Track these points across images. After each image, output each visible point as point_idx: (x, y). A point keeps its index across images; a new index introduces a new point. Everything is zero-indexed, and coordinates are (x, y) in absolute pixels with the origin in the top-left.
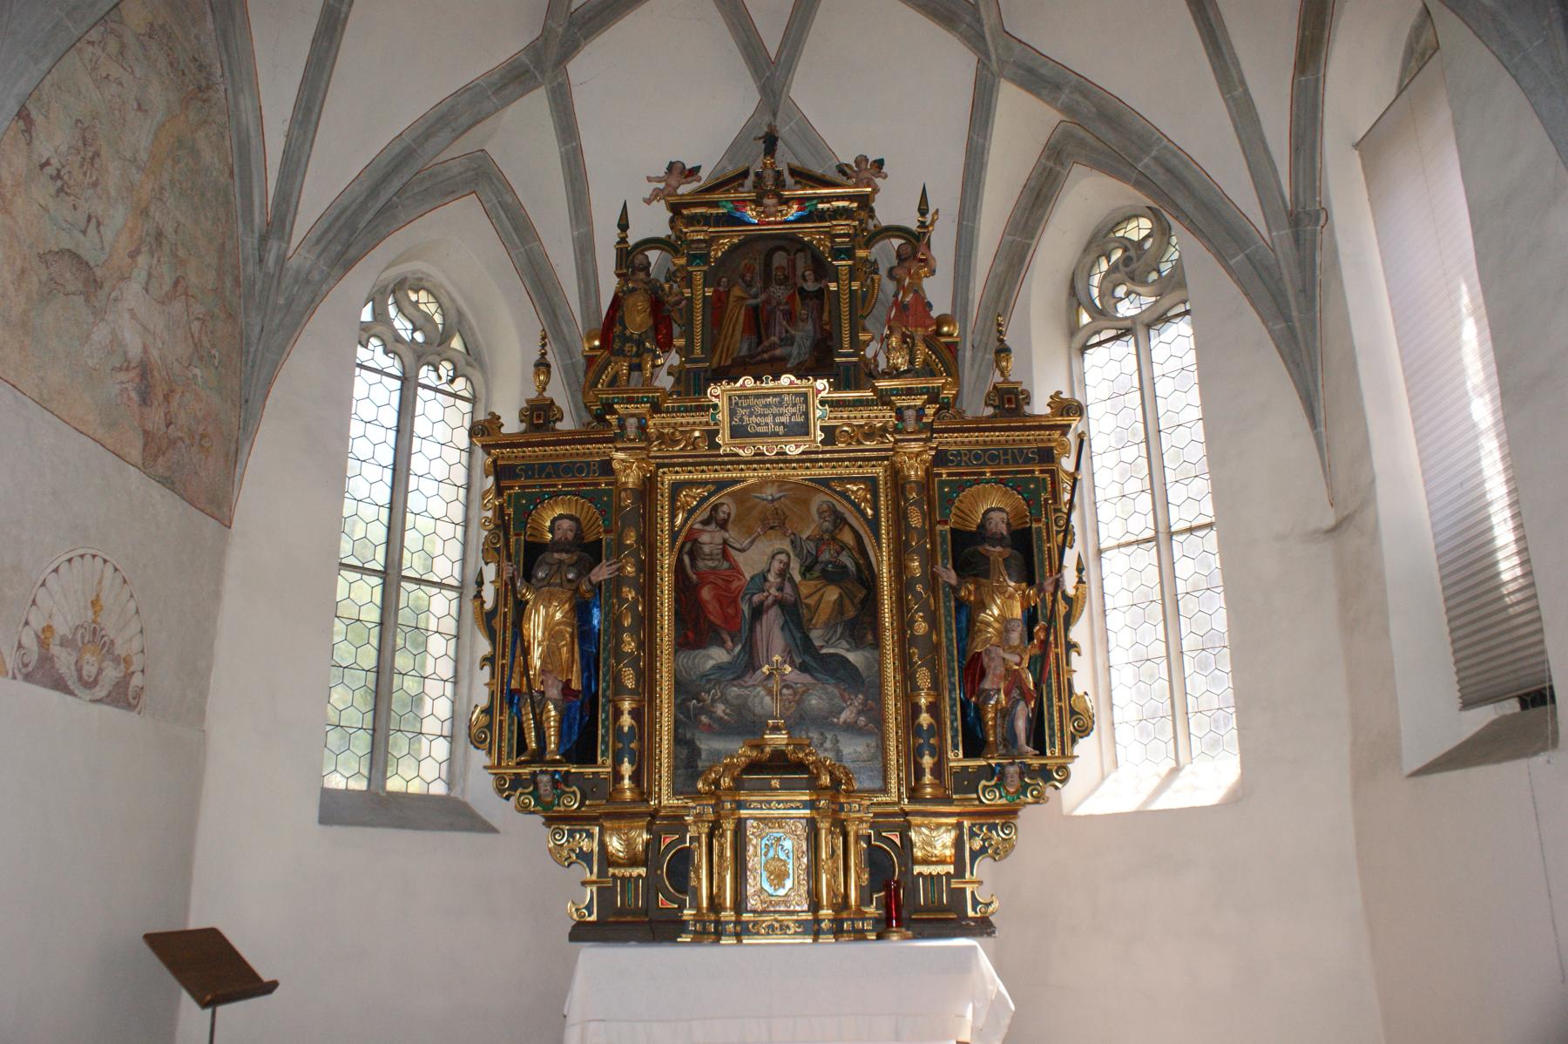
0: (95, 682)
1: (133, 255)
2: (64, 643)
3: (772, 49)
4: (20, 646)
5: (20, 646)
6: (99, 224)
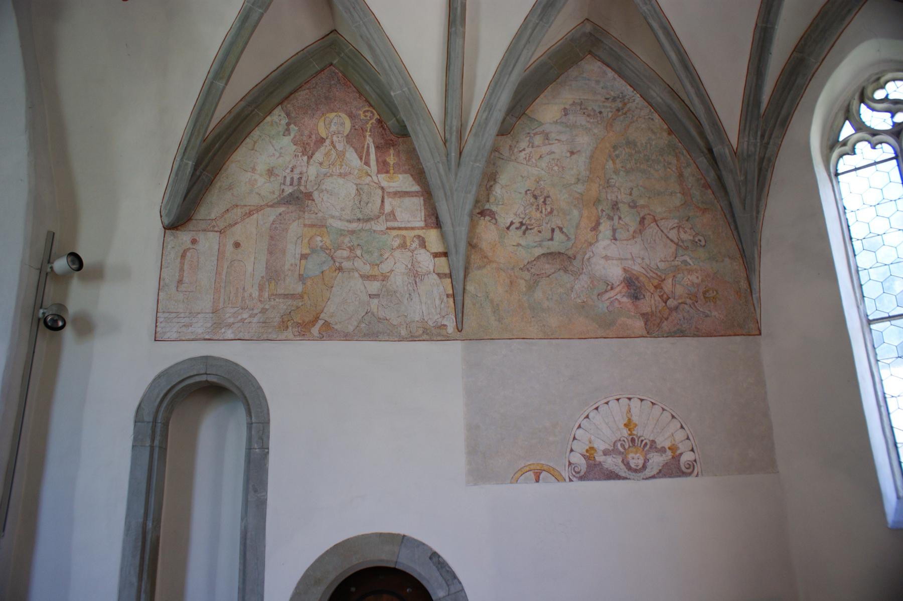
0: (644, 467)
1: (595, 228)
2: (606, 453)
3: (726, 95)
4: (570, 464)
5: (570, 464)
6: (561, 229)
